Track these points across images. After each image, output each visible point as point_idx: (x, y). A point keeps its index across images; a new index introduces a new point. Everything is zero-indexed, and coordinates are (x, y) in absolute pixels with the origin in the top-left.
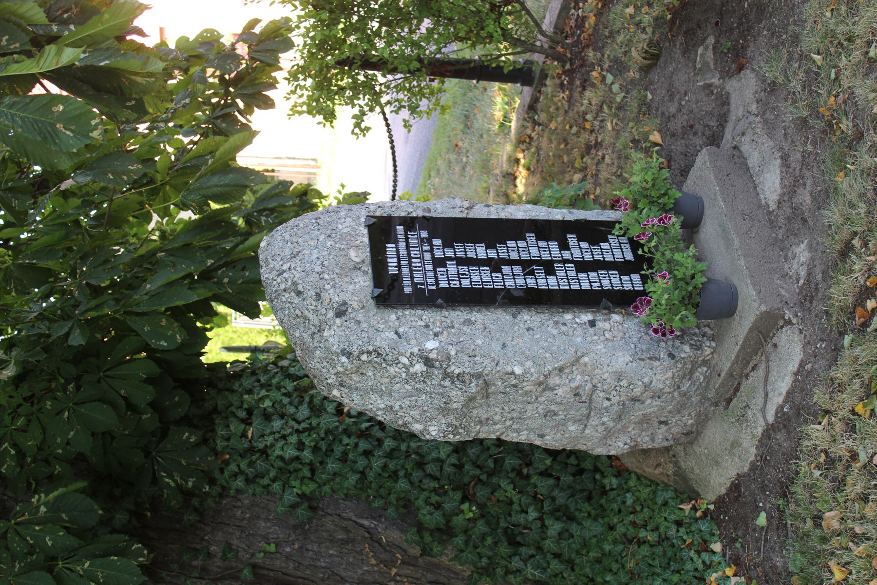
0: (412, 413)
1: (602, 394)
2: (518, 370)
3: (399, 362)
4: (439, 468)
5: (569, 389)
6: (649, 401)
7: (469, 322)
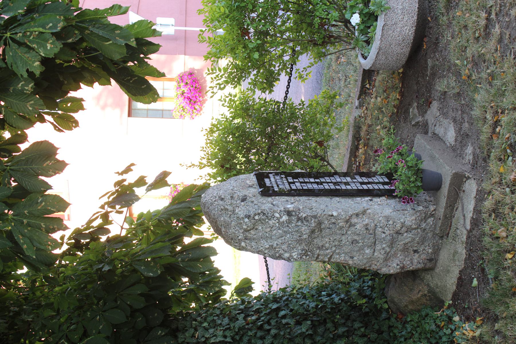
0: (283, 247)
1: (380, 229)
2: (335, 214)
3: (275, 217)
4: (302, 339)
5: (362, 226)
6: (405, 234)
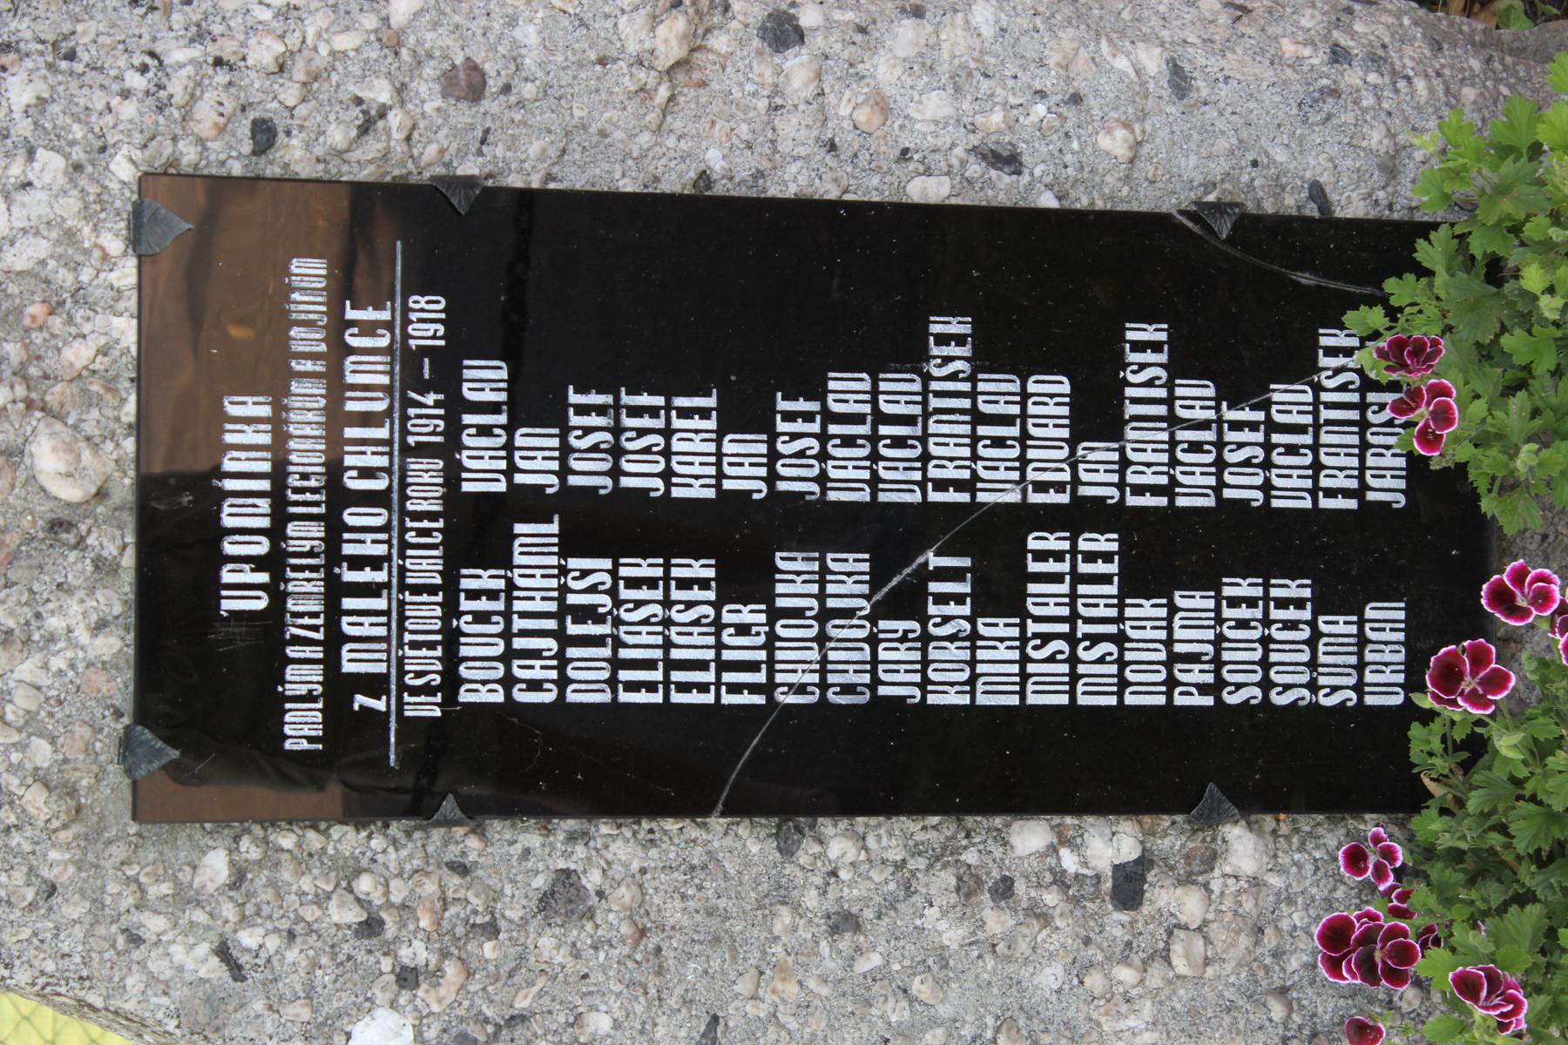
7: (563, 898)
